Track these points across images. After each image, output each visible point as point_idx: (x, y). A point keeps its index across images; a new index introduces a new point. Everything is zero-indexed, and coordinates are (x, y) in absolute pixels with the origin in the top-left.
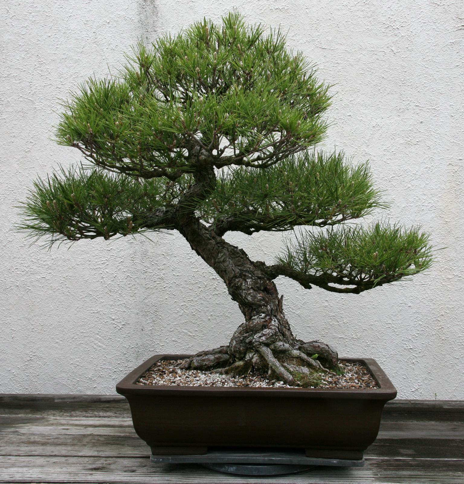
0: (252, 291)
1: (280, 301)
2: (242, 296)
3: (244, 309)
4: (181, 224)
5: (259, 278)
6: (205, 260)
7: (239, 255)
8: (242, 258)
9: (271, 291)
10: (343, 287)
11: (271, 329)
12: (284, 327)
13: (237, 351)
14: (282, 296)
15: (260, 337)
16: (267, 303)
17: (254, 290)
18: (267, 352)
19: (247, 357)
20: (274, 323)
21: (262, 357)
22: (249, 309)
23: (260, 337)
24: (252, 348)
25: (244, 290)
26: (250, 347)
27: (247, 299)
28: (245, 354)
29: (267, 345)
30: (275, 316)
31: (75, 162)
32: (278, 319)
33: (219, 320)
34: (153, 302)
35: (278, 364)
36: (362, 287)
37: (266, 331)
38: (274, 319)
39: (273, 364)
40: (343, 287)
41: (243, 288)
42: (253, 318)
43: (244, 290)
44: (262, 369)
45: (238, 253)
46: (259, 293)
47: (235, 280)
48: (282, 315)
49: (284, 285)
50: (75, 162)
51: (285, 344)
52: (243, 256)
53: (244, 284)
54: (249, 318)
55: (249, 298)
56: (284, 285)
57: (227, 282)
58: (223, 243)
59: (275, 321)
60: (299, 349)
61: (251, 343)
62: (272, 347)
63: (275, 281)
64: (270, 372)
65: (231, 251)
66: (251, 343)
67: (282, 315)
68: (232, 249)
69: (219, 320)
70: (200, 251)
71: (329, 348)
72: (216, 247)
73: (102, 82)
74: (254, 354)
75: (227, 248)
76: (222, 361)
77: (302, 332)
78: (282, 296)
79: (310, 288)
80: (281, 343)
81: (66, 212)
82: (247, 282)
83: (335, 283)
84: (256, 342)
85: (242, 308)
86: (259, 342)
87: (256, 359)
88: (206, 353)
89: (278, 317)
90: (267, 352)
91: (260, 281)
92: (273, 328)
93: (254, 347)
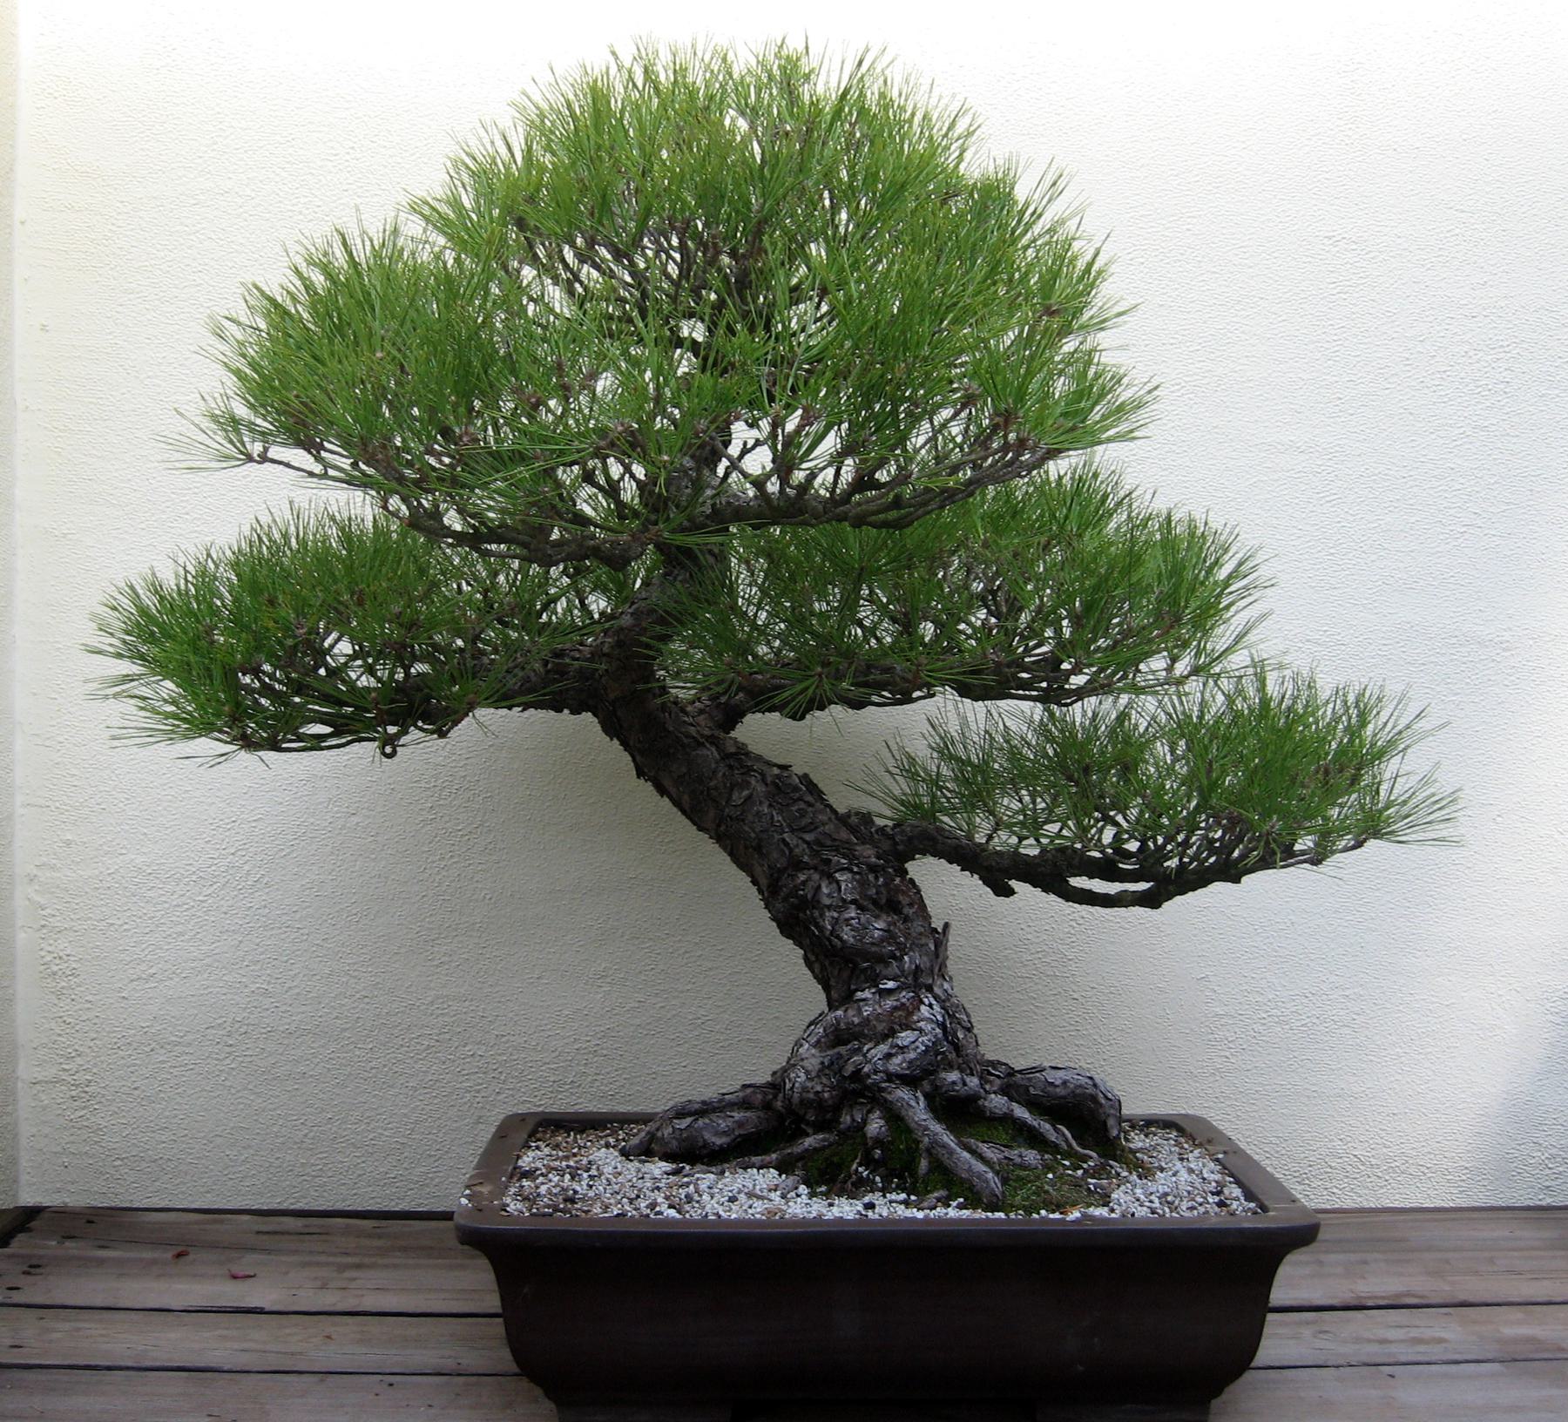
0: (852, 912)
1: (940, 937)
2: (821, 929)
3: (823, 968)
4: (612, 696)
5: (873, 869)
6: (684, 812)
7: (795, 791)
8: (810, 805)
9: (900, 901)
10: (1112, 888)
11: (921, 1030)
12: (955, 1025)
13: (811, 1102)
14: (946, 926)
15: (888, 1056)
16: (903, 950)
17: (861, 908)
18: (918, 1111)
19: (846, 1119)
20: (929, 1011)
21: (895, 1118)
22: (838, 967)
23: (888, 1056)
24: (860, 1094)
25: (829, 907)
26: (858, 1090)
27: (838, 937)
28: (837, 1109)
29: (910, 1081)
30: (930, 989)
31: (305, 497)
32: (936, 997)
33: (751, 1010)
34: (569, 986)
35: (948, 1139)
36: (1164, 886)
37: (905, 1037)
38: (928, 999)
39: (936, 1142)
40: (1112, 888)
41: (827, 901)
42: (859, 995)
43: (829, 907)
44: (901, 1165)
45: (796, 789)
46: (877, 917)
47: (793, 877)
48: (946, 986)
49: (943, 886)
50: (305, 497)
51: (968, 1080)
52: (809, 798)
53: (825, 890)
54: (839, 996)
55: (847, 935)
56: (943, 886)
57: (764, 882)
58: (742, 752)
59: (930, 1006)
60: (1004, 1091)
61: (857, 1075)
62: (926, 1085)
63: (910, 866)
64: (924, 1164)
65: (774, 783)
66: (857, 1075)
67: (946, 986)
68: (778, 777)
69: (751, 1010)
70: (667, 783)
71: (1095, 1085)
72: (722, 770)
73: (128, 679)
74: (869, 1112)
75: (763, 775)
76: (769, 1126)
77: (1016, 1037)
78: (946, 926)
79: (1009, 892)
80: (953, 1076)
81: (245, 659)
82: (838, 882)
83: (1091, 877)
84: (876, 1072)
85: (817, 967)
86: (886, 1072)
87: (876, 1125)
88: (705, 1109)
89: (936, 989)
90: (918, 1111)
91: (877, 878)
92: (928, 1027)
93: (867, 1088)
